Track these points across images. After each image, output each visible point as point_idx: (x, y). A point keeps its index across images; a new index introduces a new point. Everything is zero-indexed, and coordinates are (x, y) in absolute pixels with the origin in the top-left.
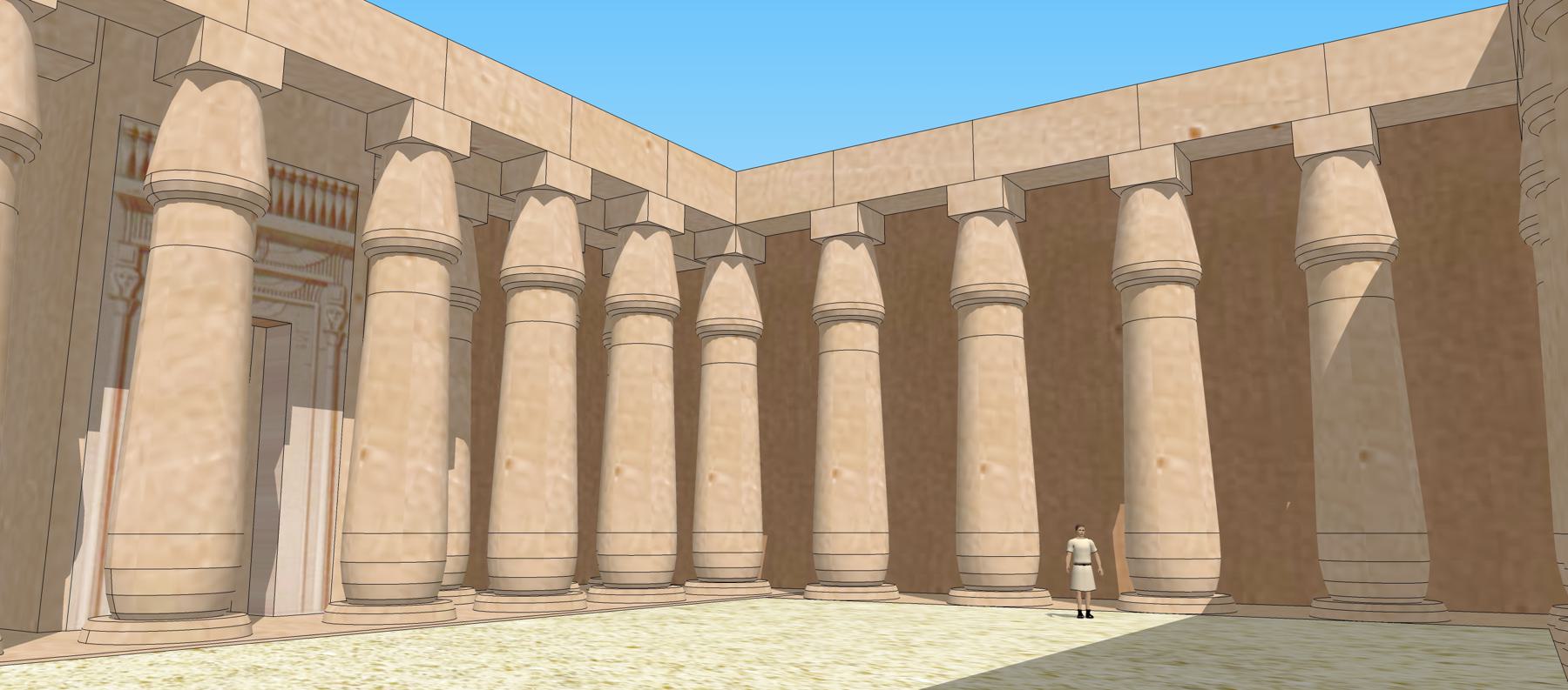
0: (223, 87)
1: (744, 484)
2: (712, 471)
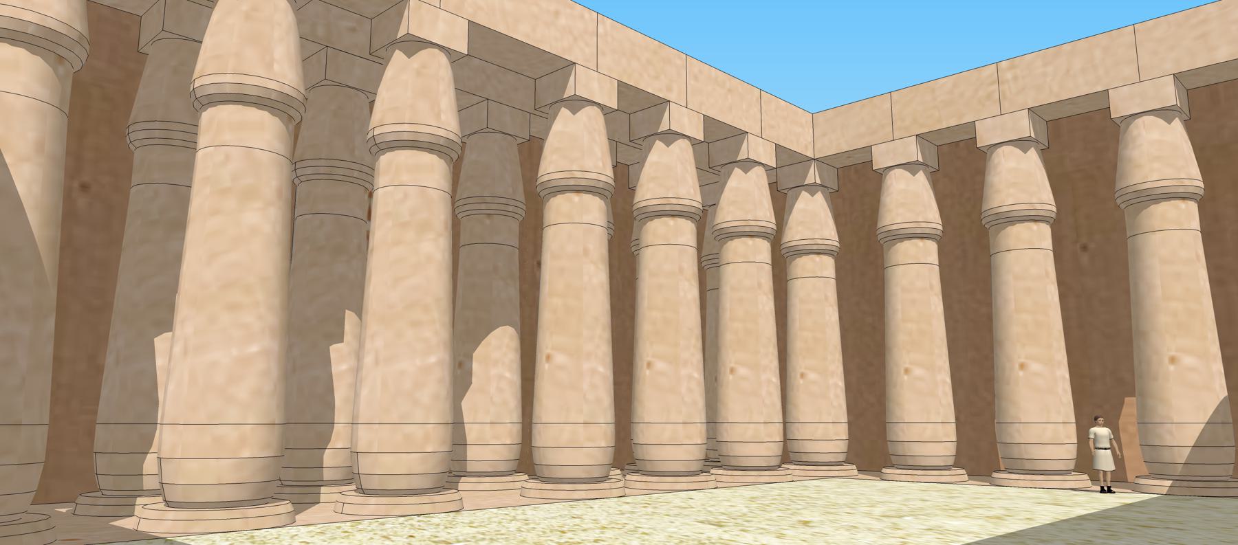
0: (424, 55)
1: (684, 372)
2: (732, 365)
